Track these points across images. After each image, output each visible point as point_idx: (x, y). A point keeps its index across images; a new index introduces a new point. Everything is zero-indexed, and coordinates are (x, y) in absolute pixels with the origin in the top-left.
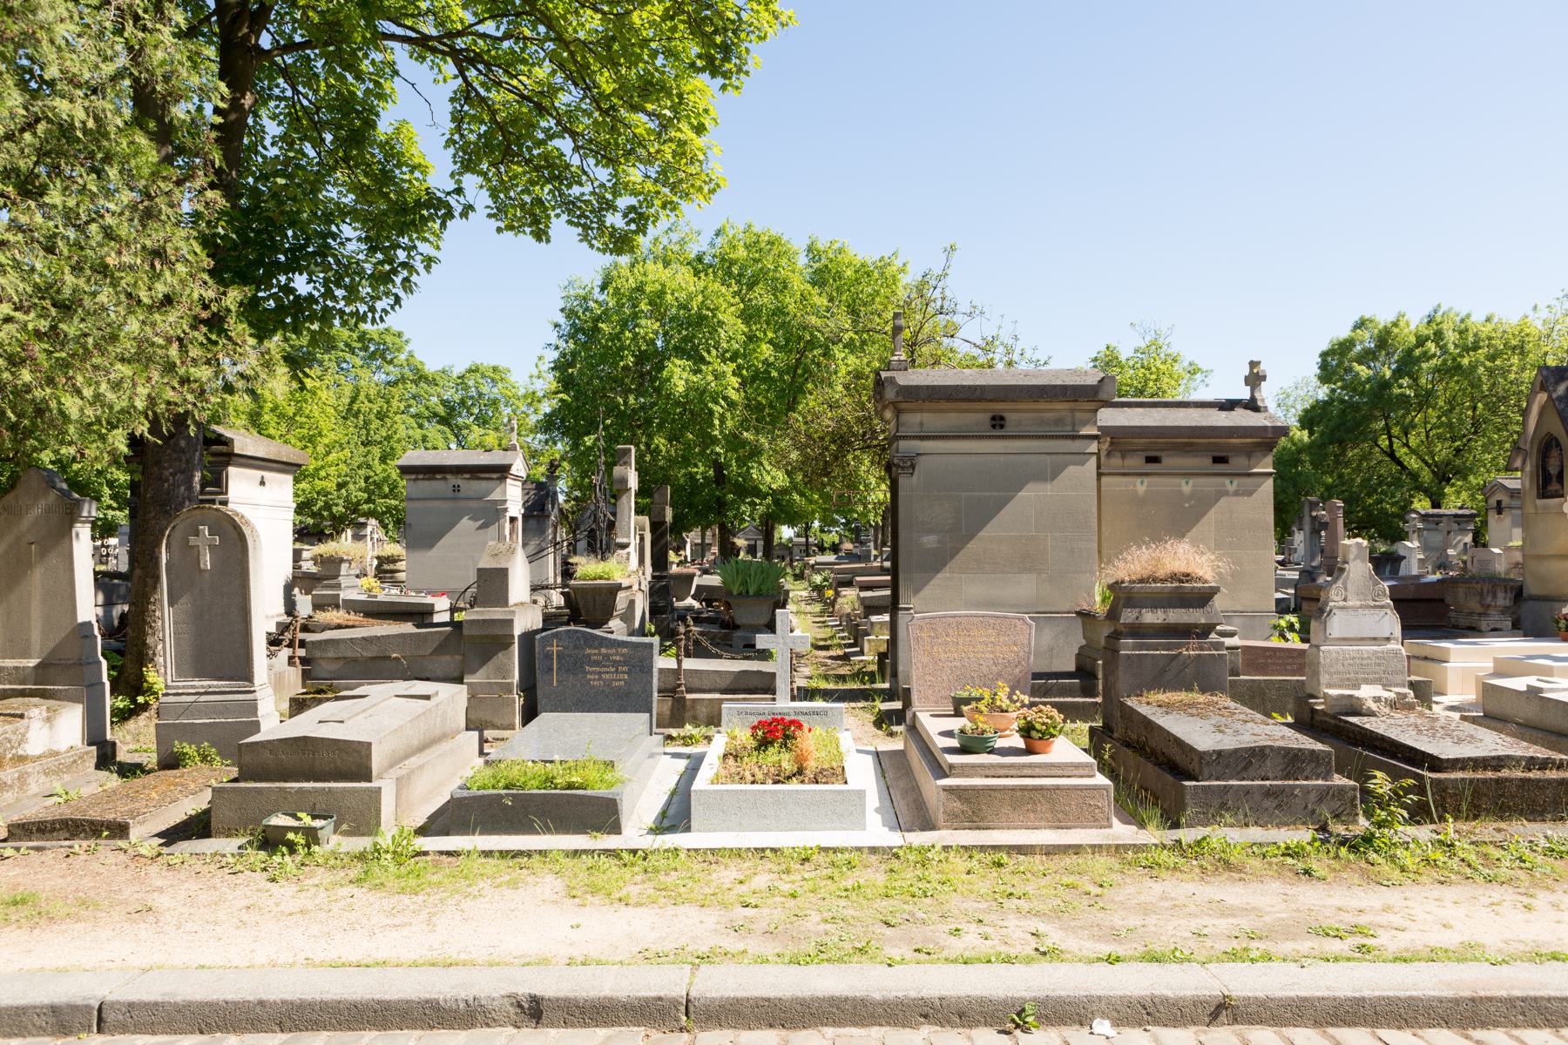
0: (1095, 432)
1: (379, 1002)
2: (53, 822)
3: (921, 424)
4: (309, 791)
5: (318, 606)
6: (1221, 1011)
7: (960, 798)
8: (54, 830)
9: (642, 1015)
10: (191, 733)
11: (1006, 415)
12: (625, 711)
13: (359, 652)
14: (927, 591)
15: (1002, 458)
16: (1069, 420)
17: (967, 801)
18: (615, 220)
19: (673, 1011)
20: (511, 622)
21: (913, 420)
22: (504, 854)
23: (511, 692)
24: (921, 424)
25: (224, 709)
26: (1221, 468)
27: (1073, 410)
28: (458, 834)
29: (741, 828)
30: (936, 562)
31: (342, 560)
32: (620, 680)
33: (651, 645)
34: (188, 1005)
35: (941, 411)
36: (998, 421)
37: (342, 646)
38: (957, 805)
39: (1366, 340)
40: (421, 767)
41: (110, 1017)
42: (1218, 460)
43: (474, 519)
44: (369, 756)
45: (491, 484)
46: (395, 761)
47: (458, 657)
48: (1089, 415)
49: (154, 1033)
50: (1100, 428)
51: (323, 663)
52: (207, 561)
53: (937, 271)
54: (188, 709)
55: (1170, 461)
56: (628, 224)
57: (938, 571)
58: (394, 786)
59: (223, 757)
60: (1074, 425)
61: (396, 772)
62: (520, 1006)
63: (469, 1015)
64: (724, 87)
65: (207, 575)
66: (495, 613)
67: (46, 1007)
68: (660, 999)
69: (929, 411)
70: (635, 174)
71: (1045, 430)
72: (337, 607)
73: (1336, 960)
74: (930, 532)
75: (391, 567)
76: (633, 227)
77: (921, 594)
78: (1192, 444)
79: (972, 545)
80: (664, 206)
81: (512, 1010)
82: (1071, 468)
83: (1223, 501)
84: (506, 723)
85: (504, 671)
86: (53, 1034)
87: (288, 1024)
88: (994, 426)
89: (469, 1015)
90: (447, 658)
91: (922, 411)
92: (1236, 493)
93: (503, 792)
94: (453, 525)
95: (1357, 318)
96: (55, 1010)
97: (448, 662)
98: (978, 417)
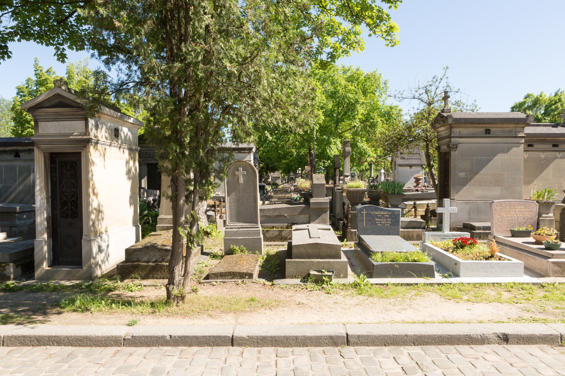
0: (523, 135)
1: (449, 335)
2: (226, 273)
3: (460, 132)
4: (321, 262)
6: (232, 341)
7: (558, 266)
8: (226, 275)
9: (545, 341)
10: (237, 242)
11: (491, 129)
14: (460, 193)
15: (489, 145)
16: (514, 131)
17: (561, 267)
18: (324, 57)
19: (556, 340)
21: (456, 131)
22: (408, 285)
24: (460, 132)
25: (248, 233)
26: (555, 148)
27: (516, 127)
28: (376, 277)
29: (478, 276)
30: (464, 182)
34: (380, 336)
35: (468, 127)
36: (488, 131)
38: (557, 268)
39: (529, 102)
41: (351, 340)
42: (554, 146)
45: (245, 155)
47: (307, 216)
48: (522, 129)
49: (368, 346)
50: (525, 134)
52: (241, 180)
53: (439, 76)
54: (235, 234)
55: (536, 146)
56: (328, 59)
57: (465, 185)
59: (249, 250)
60: (516, 133)
62: (499, 337)
63: (482, 340)
64: (390, 7)
65: (241, 185)
67: (328, 336)
68: (551, 335)
69: (463, 127)
70: (331, 40)
71: (505, 135)
73: (407, 323)
74: (462, 171)
76: (329, 60)
77: (458, 194)
78: (545, 140)
79: (477, 176)
80: (343, 52)
81: (496, 338)
82: (514, 149)
83: (556, 161)
86: (331, 346)
87: (417, 343)
88: (486, 133)
89: (482, 340)
90: (303, 216)
91: (460, 127)
92: (561, 158)
95: (526, 94)
96: (331, 337)
98: (480, 130)
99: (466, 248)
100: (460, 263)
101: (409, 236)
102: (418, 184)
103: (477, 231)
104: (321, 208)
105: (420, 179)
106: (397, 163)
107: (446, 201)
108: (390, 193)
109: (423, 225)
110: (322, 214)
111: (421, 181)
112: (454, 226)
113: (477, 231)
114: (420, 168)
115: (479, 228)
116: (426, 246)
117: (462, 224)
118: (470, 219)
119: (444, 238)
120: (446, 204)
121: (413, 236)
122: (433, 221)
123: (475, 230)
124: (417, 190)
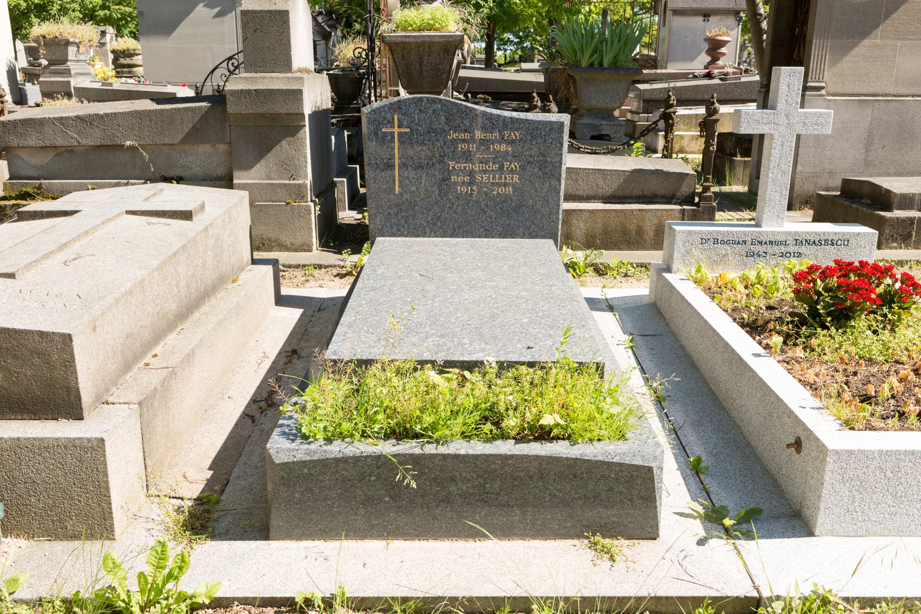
5: (48, 94)
12: (513, 236)
13: (73, 138)
20: (299, 93)
23: (303, 198)
28: (288, 535)
30: (860, 27)
31: (68, 43)
32: (508, 182)
33: (562, 124)
37: (48, 129)
40: (189, 357)
43: (210, 5)
44: (69, 363)
46: (133, 356)
47: (222, 147)
51: (24, 155)
57: (864, 38)
58: (135, 422)
61: (141, 381)
66: (273, 81)
72: (69, 95)
75: (128, 61)
84: (298, 242)
85: (290, 168)
93: (388, 448)
94: (188, 13)
97: (207, 155)
99: (861, 322)
100: (822, 450)
101: (625, 232)
102: (715, 59)
103: (898, 214)
104: (275, 117)
105: (723, 44)
106: (670, 6)
107: (788, 78)
108: (584, 63)
109: (685, 190)
110: (278, 142)
111: (723, 50)
112: (806, 188)
113: (898, 214)
114: (731, 20)
115: (907, 202)
116: (671, 288)
117: (838, 183)
118: (868, 163)
119: (757, 248)
120: (783, 89)
121: (640, 231)
122: (739, 171)
123: (889, 209)
124: (709, 76)
